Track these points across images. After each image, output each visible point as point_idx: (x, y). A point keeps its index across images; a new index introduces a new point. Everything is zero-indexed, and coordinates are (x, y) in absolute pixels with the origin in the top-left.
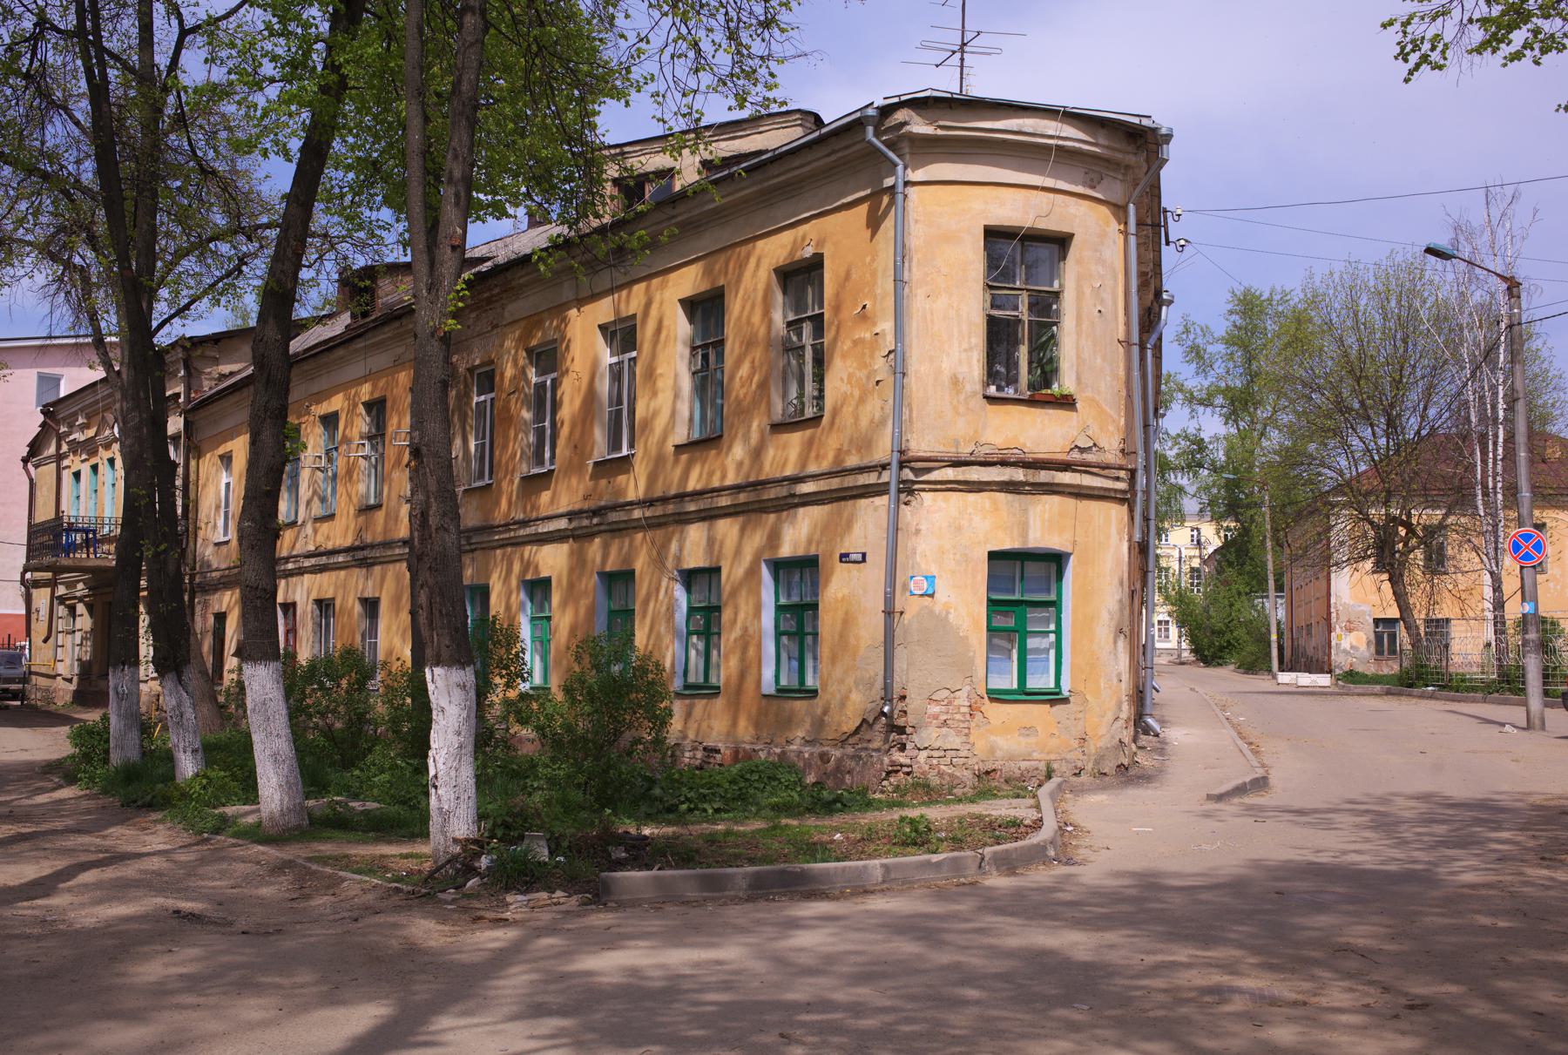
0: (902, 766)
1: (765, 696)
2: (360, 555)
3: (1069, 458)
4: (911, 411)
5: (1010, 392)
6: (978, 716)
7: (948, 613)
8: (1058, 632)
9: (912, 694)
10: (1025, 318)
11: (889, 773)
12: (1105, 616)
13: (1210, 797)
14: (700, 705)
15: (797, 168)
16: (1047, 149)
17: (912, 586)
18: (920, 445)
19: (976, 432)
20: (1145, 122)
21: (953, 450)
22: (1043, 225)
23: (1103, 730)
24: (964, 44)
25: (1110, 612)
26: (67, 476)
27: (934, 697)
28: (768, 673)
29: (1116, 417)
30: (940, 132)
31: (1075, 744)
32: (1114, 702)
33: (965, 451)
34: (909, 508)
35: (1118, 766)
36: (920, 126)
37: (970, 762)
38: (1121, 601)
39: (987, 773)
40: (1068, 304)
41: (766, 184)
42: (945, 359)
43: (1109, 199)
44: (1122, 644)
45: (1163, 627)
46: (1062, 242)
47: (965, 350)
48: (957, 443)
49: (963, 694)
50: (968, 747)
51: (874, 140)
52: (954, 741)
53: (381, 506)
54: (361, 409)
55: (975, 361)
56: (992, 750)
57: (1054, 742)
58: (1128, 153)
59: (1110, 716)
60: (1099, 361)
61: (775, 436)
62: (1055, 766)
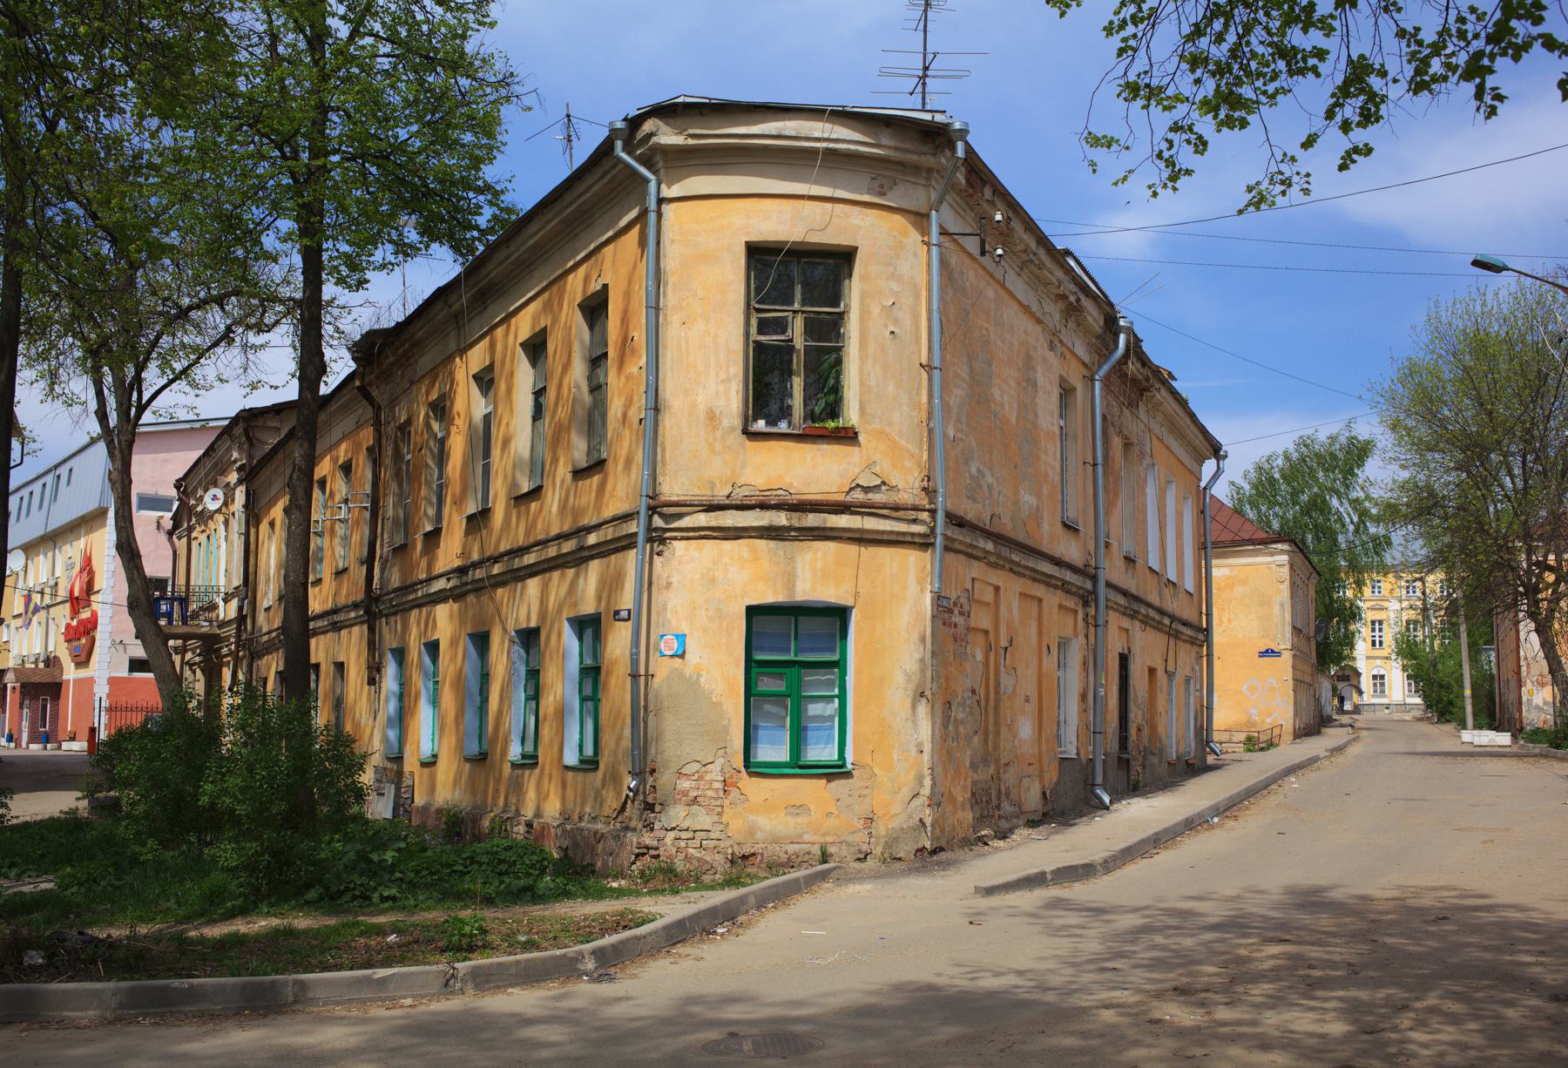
0: (648, 848)
1: (567, 768)
2: (336, 618)
3: (849, 498)
4: (664, 450)
5: (783, 427)
6: (734, 792)
7: (699, 676)
8: (842, 697)
10: (799, 343)
11: (637, 856)
12: (900, 678)
13: (978, 890)
15: (582, 194)
16: (813, 152)
18: (673, 488)
19: (733, 472)
20: (939, 118)
21: (709, 493)
22: (815, 238)
23: (896, 808)
24: (926, 68)
25: (905, 671)
26: (194, 544)
27: (683, 771)
29: (917, 451)
30: (691, 142)
31: (859, 824)
32: (911, 776)
33: (721, 494)
34: (661, 559)
35: (917, 851)
36: (668, 136)
38: (922, 660)
39: (744, 857)
40: (852, 328)
42: (701, 391)
44: (923, 709)
45: (1378, 681)
46: (843, 259)
47: (723, 381)
48: (712, 485)
49: (716, 768)
50: (722, 827)
51: (624, 156)
52: (703, 819)
56: (751, 832)
57: (833, 822)
58: (925, 154)
59: (906, 793)
60: (891, 388)
62: (831, 850)
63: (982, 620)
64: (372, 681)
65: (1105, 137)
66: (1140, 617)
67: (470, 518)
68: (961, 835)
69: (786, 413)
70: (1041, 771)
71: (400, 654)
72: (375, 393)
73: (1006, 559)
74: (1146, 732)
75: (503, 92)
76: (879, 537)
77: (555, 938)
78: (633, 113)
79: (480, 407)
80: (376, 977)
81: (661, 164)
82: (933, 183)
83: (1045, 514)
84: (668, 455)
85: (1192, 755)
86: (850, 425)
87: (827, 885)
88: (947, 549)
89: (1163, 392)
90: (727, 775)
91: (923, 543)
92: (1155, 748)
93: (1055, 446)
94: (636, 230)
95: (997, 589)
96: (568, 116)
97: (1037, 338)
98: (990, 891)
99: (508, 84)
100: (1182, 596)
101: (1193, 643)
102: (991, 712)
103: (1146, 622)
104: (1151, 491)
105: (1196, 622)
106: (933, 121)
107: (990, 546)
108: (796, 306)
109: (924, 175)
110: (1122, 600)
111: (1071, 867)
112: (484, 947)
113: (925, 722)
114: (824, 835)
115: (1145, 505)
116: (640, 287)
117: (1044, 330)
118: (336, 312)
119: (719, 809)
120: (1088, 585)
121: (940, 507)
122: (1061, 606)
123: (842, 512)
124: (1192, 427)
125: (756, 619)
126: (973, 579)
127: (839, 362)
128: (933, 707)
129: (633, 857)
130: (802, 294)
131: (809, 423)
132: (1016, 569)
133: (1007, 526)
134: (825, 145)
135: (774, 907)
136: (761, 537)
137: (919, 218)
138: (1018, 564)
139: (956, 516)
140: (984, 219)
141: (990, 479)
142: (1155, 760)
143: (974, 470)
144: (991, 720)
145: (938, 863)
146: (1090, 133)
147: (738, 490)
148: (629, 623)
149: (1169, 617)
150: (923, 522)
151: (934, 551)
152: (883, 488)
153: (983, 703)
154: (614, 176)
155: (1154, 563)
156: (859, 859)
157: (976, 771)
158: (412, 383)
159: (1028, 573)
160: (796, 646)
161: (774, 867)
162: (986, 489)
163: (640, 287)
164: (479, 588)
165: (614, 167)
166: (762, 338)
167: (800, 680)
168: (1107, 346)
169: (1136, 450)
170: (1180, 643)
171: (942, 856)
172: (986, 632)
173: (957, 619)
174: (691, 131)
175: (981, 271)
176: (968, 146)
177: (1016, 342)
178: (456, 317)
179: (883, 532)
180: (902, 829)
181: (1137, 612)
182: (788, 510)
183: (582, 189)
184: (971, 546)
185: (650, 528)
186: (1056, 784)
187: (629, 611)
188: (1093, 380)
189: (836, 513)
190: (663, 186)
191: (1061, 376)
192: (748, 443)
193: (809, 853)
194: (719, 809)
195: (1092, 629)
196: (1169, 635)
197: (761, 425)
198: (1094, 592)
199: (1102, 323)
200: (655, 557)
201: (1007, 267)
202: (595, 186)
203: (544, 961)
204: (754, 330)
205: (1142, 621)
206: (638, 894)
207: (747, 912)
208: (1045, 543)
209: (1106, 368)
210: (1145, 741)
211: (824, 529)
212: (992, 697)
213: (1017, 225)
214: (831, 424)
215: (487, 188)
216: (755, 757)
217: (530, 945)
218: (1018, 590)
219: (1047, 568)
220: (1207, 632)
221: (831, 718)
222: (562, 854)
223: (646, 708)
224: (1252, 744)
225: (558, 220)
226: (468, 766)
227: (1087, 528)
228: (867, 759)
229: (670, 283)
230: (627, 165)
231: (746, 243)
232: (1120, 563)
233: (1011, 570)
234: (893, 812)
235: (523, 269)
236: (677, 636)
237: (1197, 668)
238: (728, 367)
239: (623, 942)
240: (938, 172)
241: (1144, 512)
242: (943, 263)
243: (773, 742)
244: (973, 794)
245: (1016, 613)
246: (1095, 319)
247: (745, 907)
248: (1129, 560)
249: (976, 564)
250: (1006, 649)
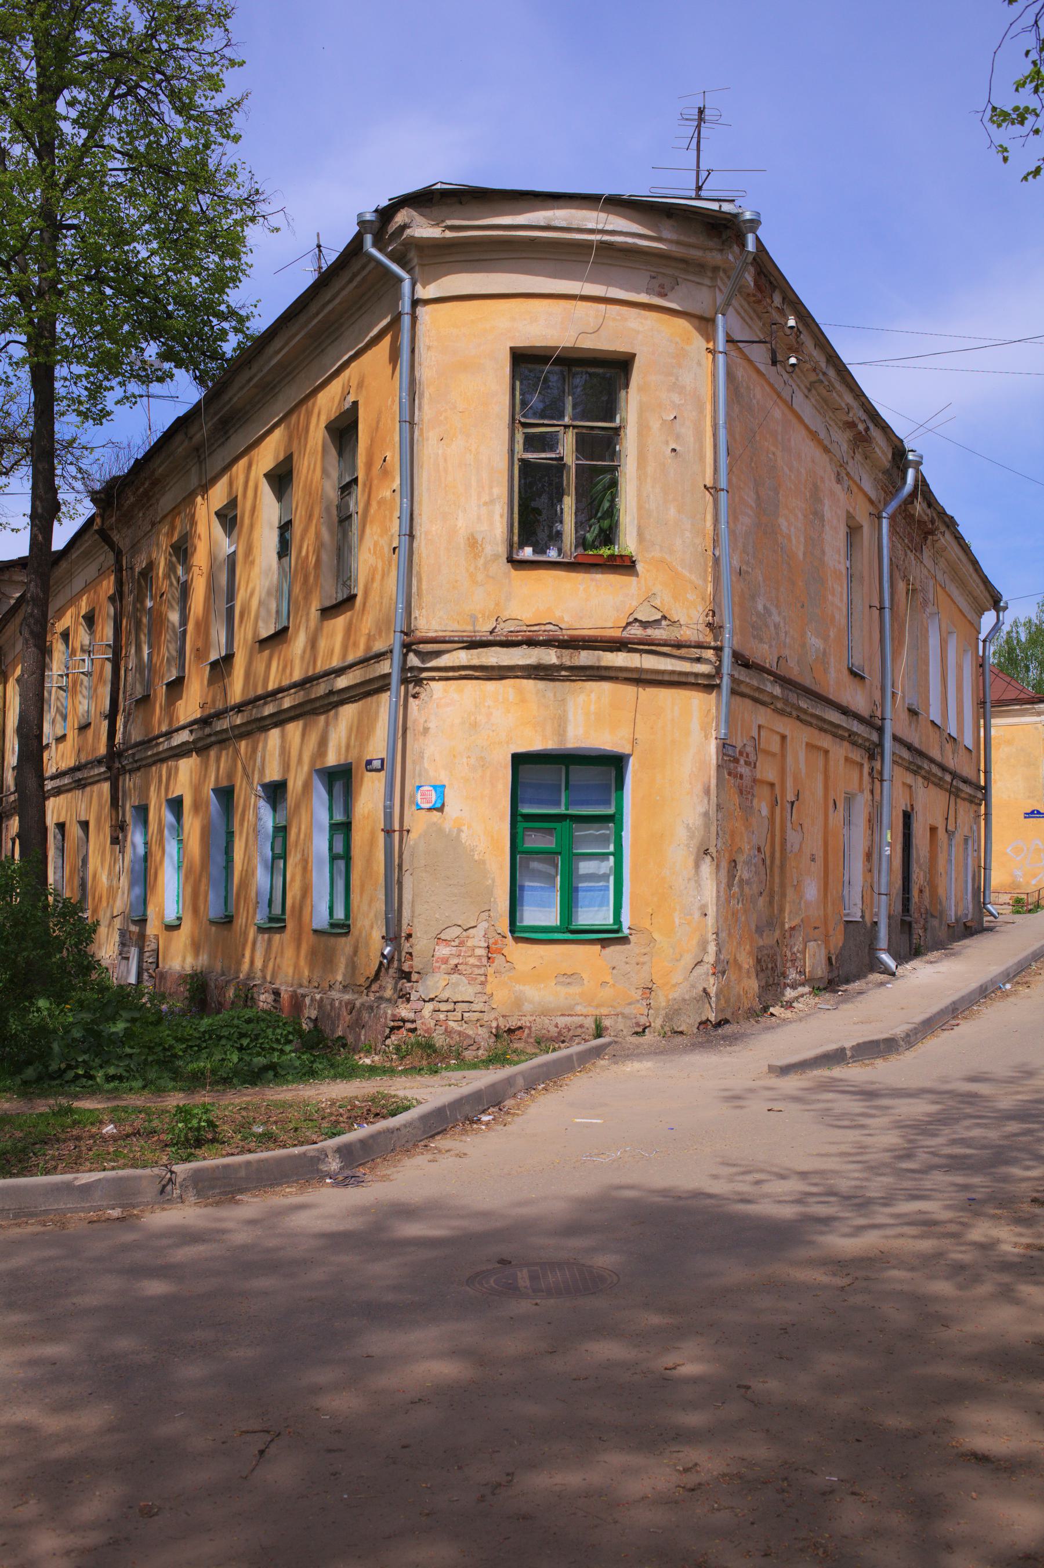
0: (404, 1021)
1: (315, 931)
2: (79, 775)
3: (625, 634)
4: (420, 581)
5: (552, 555)
6: (499, 960)
7: (460, 831)
8: (618, 854)
9: (418, 933)
10: (570, 459)
11: (393, 1029)
12: (682, 833)
13: (772, 1069)
14: (277, 937)
16: (584, 247)
17: (419, 796)
19: (497, 604)
20: (727, 207)
21: (470, 628)
22: (588, 343)
23: (677, 977)
25: (688, 827)
27: (442, 936)
28: (323, 908)
29: (700, 582)
30: (449, 234)
31: (637, 995)
32: (694, 942)
33: (483, 629)
34: (417, 702)
35: (701, 1023)
37: (486, 1017)
38: (706, 814)
39: (510, 1031)
40: (629, 445)
41: (310, 326)
43: (690, 310)
44: (707, 868)
47: (486, 504)
48: (474, 619)
49: (478, 933)
50: (485, 998)
52: (465, 990)
53: (90, 724)
54: (81, 620)
55: (497, 517)
56: (518, 1002)
57: (606, 993)
58: (711, 250)
59: (688, 960)
60: (672, 511)
61: (326, 623)
62: (607, 1022)
63: (768, 772)
64: (115, 841)
65: (1016, 109)
66: (923, 773)
67: (214, 665)
68: (747, 1006)
69: (557, 537)
70: (827, 936)
71: (142, 811)
72: (116, 537)
73: (793, 706)
74: (927, 894)
75: (250, 213)
76: (660, 678)
77: (296, 1130)
78: (384, 203)
79: (225, 546)
80: (77, 1183)
81: (415, 261)
82: (719, 283)
83: (832, 660)
84: (424, 587)
85: (970, 917)
86: (626, 553)
87: (602, 1062)
88: (733, 692)
89: (948, 536)
90: (491, 941)
91: (708, 685)
92: (934, 912)
93: (842, 587)
94: (387, 341)
95: (783, 738)
96: (319, 246)
97: (825, 470)
98: (785, 1070)
99: (253, 202)
100: (962, 752)
101: (971, 802)
102: (777, 871)
103: (929, 778)
104: (934, 642)
105: (974, 780)
106: (720, 211)
107: (777, 691)
108: (567, 420)
109: (709, 274)
110: (906, 754)
111: (871, 1042)
112: (213, 1141)
113: (709, 882)
114: (598, 1006)
115: (927, 655)
116: (393, 401)
117: (831, 460)
118: (77, 452)
119: (483, 978)
120: (875, 737)
121: (726, 644)
122: (847, 759)
123: (619, 650)
124: (975, 576)
125: (524, 769)
126: (759, 727)
127: (614, 484)
128: (718, 866)
129: (387, 1031)
130: (574, 407)
131: (580, 550)
132: (803, 716)
133: (794, 670)
134: (598, 237)
135: (545, 1089)
136: (528, 677)
137: (705, 323)
138: (805, 712)
139: (743, 656)
140: (774, 327)
141: (777, 618)
142: (935, 923)
143: (760, 607)
144: (777, 880)
145: (724, 1038)
146: (994, 109)
147: (502, 625)
148: (383, 773)
149: (951, 773)
150: (707, 661)
151: (719, 695)
152: (664, 623)
153: (768, 862)
154: (364, 279)
155: (935, 715)
156: (636, 1033)
157: (761, 936)
158: (153, 524)
159: (814, 722)
160: (567, 798)
161: (544, 1042)
162: (772, 628)
163: (393, 401)
164: (223, 740)
165: (363, 267)
166: (529, 456)
167: (571, 836)
168: (893, 484)
169: (920, 595)
170: (959, 800)
171: (727, 1029)
172: (772, 785)
173: (743, 769)
174: (449, 223)
175: (767, 389)
176: (758, 240)
177: (803, 471)
178: (197, 450)
179: (663, 672)
180: (684, 1000)
181: (920, 767)
182: (558, 647)
183: (328, 297)
184: (758, 689)
185: (404, 668)
186: (842, 948)
187: (382, 760)
188: (880, 518)
189: (611, 650)
190: (419, 287)
191: (848, 512)
192: (514, 573)
193: (581, 1026)
194: (483, 978)
195: (877, 783)
196: (950, 792)
197: (528, 553)
198: (881, 745)
199: (890, 456)
200: (411, 700)
201: (795, 387)
202: (343, 291)
203: (280, 1161)
204: (519, 446)
205: (924, 778)
206: (391, 1072)
207: (515, 1096)
208: (831, 690)
209: (894, 505)
210: (927, 903)
211: (599, 668)
212: (778, 855)
213: (806, 339)
214: (605, 552)
215: (232, 313)
216: (522, 921)
217: (268, 1139)
218: (805, 740)
219: (834, 717)
220: (986, 789)
221: (605, 877)
222: (311, 1025)
223: (400, 866)
224: (1020, 906)
225: (302, 334)
226: (213, 929)
227: (873, 678)
228: (646, 923)
229: (427, 395)
230: (379, 263)
231: (511, 348)
232: (904, 715)
233: (798, 718)
234: (674, 981)
235: (268, 389)
236: (435, 787)
237: (975, 827)
238: (491, 487)
239: (374, 1137)
240: (725, 271)
241: (927, 664)
242: (730, 375)
243: (543, 904)
244: (759, 961)
245: (802, 766)
246: (883, 452)
247: (513, 1090)
248: (913, 712)
249: (762, 709)
250: (792, 803)
